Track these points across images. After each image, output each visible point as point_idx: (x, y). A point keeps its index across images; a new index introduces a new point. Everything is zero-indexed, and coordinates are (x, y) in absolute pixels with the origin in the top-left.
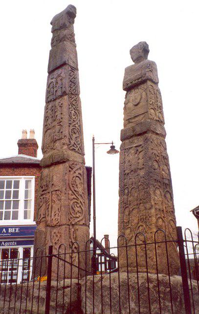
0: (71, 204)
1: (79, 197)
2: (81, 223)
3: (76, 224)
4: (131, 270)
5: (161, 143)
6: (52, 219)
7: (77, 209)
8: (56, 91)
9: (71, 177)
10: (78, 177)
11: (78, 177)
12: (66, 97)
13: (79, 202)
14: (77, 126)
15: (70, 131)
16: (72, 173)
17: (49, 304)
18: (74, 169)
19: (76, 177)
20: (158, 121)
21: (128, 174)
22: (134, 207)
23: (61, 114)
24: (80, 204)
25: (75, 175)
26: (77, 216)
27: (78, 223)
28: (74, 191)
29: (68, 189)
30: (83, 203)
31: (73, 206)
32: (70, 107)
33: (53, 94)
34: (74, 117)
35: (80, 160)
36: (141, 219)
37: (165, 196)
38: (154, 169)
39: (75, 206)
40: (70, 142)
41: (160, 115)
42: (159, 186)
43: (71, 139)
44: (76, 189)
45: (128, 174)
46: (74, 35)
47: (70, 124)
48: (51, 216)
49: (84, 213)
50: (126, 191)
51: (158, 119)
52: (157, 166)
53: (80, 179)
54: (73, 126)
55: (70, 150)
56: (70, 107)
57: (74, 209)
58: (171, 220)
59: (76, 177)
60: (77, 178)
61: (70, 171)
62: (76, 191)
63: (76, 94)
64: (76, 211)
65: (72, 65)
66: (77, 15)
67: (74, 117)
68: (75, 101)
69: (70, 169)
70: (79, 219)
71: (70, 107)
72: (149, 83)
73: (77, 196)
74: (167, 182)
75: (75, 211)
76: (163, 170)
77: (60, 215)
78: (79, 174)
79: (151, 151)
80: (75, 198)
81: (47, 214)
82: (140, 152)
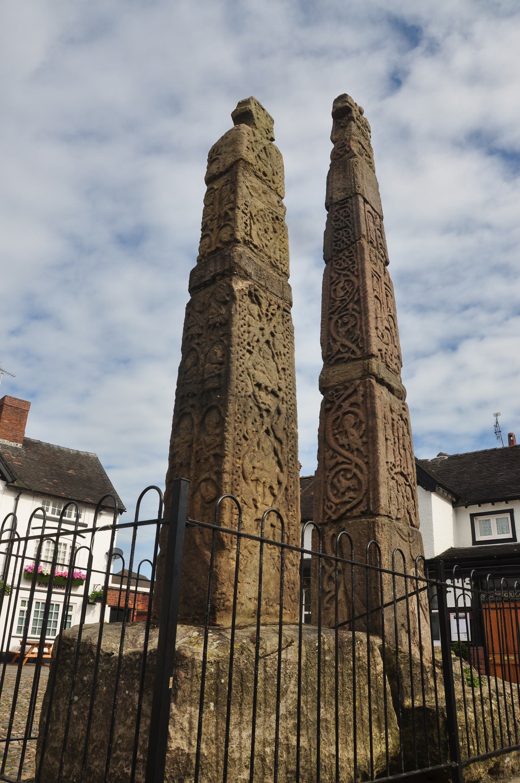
2: (356, 512)
26: (346, 498)
31: (335, 480)
53: (356, 415)
62: (342, 446)
70: (348, 506)
73: (346, 453)
80: (340, 459)
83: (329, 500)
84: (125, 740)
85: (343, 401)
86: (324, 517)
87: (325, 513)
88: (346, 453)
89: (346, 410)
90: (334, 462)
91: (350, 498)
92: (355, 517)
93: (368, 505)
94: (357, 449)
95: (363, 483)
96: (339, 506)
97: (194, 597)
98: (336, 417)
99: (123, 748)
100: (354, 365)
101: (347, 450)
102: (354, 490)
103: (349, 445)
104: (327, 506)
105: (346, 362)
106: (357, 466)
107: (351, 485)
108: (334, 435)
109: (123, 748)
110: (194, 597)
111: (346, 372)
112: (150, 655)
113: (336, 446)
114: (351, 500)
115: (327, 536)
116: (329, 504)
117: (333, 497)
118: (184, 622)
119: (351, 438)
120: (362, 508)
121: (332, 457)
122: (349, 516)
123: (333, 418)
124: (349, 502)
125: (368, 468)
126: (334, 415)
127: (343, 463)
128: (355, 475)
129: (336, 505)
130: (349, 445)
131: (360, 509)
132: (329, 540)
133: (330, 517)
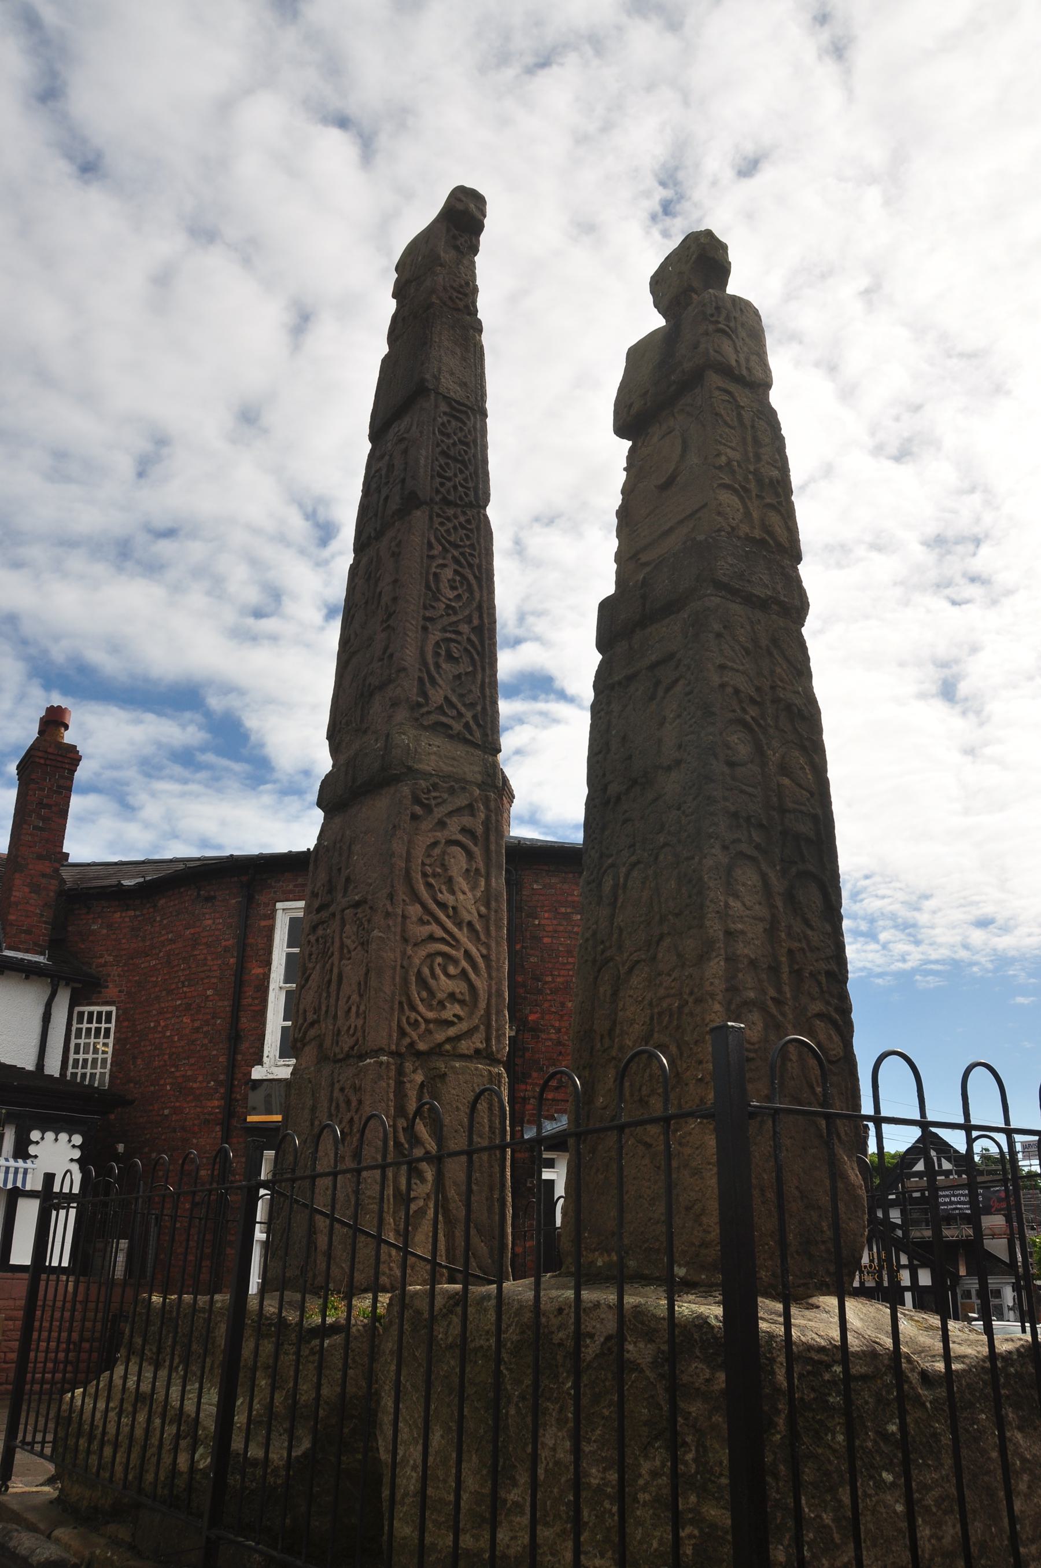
0: (417, 961)
1: (462, 936)
2: (465, 1046)
3: (436, 1050)
4: (486, 1310)
5: (774, 641)
6: (339, 1031)
7: (445, 985)
8: (387, 498)
9: (423, 841)
10: (457, 843)
11: (457, 843)
12: (419, 515)
13: (459, 954)
14: (465, 628)
15: (429, 649)
16: (425, 825)
17: (623, 1348)
18: (439, 812)
19: (451, 842)
20: (762, 542)
21: (618, 799)
22: (635, 957)
23: (396, 581)
24: (464, 964)
25: (441, 836)
26: (447, 1014)
27: (448, 1047)
28: (433, 906)
29: (401, 895)
30: (480, 961)
31: (426, 971)
32: (437, 550)
33: (376, 515)
34: (451, 594)
35: (472, 771)
36: (660, 1014)
37: (790, 897)
38: (731, 764)
39: (438, 971)
40: (424, 694)
41: (774, 519)
42: (757, 847)
43: (433, 682)
44: (446, 897)
45: (618, 799)
46: (475, 290)
47: (427, 619)
48: (335, 1017)
49: (482, 1005)
50: (608, 884)
51: (757, 534)
52: (743, 750)
53: (470, 855)
54: (444, 630)
55: (426, 728)
56: (435, 552)
57: (432, 982)
58: (820, 1016)
59: (451, 842)
60: (456, 850)
61: (414, 817)
62: (442, 906)
63: (471, 505)
64: (440, 995)
65: (456, 392)
66: (486, 221)
67: (451, 594)
68: (462, 532)
69: (418, 810)
70: (452, 1032)
71: (435, 552)
72: (714, 379)
73: (449, 924)
74: (805, 828)
75: (432, 994)
76: (784, 769)
77: (362, 1008)
78: (464, 830)
79: (716, 680)
80: (439, 933)
81: (324, 1008)
82: (668, 690)
83: (413, 1008)
84: (1027, 1522)
85: (450, 814)
86: (399, 1040)
87: (402, 1033)
88: (449, 924)
89: (454, 837)
90: (425, 931)
91: (455, 1015)
92: (463, 1057)
93: (488, 1040)
94: (470, 924)
95: (481, 992)
96: (431, 1026)
97: (823, 1242)
98: (432, 840)
99: (1028, 1538)
100: (468, 752)
101: (448, 917)
102: (462, 1002)
103: (454, 908)
104: (408, 1018)
105: (451, 737)
106: (467, 954)
107: (458, 991)
108: (425, 875)
109: (1028, 1538)
110: (823, 1242)
111: (454, 759)
112: (1019, 1356)
113: (431, 901)
114: (456, 1020)
115: (410, 1082)
116: (413, 1015)
117: (420, 1003)
118: (767, 1295)
119: (462, 897)
120: (477, 1042)
121: (422, 922)
122: (448, 1051)
123: (429, 841)
124: (450, 1024)
125: (489, 967)
126: (430, 835)
127: (442, 940)
128: (464, 973)
129: (427, 1021)
130: (454, 908)
131: (474, 1043)
132: (415, 1093)
133: (412, 1044)
